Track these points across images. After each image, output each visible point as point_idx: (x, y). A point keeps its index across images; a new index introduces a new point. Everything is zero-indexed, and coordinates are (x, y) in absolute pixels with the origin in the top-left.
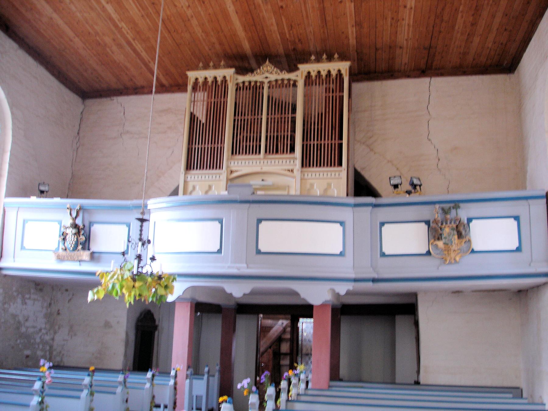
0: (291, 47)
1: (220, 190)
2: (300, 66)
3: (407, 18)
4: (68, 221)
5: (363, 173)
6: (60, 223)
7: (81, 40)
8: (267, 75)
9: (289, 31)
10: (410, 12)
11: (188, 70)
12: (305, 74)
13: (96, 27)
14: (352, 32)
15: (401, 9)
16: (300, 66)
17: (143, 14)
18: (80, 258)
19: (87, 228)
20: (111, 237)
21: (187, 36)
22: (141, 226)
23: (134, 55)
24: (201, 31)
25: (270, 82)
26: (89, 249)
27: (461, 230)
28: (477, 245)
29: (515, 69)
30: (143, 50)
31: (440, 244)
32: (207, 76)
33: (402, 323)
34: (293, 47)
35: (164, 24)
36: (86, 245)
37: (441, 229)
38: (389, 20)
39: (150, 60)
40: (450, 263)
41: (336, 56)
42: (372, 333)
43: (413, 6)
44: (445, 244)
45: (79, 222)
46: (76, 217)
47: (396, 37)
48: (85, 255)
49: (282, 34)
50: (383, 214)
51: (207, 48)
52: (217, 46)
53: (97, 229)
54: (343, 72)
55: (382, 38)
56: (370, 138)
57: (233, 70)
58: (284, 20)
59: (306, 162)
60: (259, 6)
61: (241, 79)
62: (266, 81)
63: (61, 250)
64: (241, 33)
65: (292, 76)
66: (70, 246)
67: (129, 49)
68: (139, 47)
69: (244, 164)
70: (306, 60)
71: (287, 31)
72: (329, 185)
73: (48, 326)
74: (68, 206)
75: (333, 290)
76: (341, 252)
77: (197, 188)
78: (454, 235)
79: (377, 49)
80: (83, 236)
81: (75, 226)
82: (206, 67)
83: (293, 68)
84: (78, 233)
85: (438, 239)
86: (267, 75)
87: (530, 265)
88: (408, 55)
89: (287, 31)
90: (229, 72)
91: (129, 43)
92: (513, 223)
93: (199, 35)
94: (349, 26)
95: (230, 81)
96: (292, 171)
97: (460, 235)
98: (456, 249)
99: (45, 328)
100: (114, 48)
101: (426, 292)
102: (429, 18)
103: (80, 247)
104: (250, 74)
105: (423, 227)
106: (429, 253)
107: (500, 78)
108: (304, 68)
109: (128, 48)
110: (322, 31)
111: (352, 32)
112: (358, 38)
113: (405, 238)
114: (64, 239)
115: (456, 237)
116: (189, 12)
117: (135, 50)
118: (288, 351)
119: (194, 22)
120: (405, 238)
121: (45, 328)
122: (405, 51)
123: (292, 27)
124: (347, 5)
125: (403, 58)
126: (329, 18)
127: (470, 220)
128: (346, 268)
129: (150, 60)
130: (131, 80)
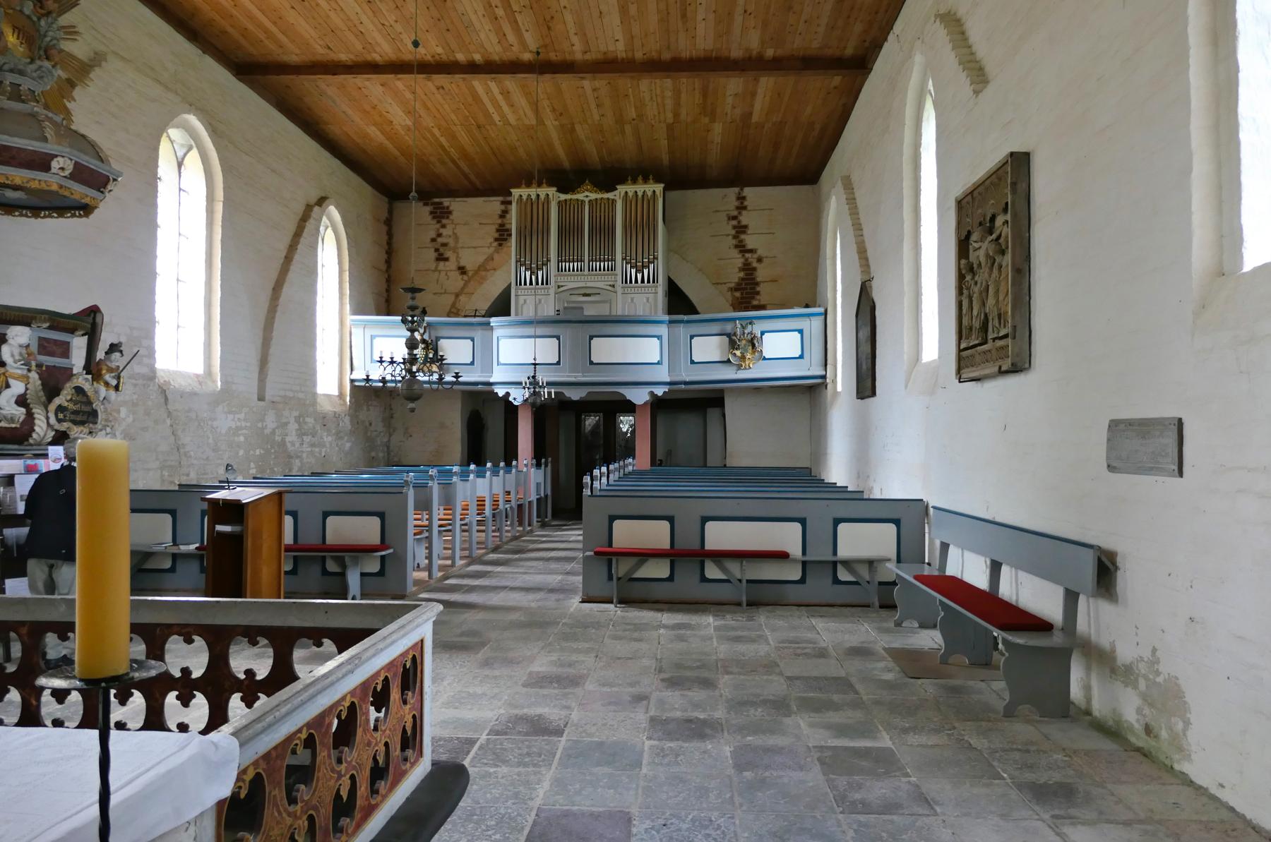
8: (587, 195)
27: (753, 343)
28: (766, 354)
31: (738, 353)
33: (713, 414)
35: (657, 602)
42: (686, 426)
50: (695, 329)
54: (658, 193)
61: (563, 197)
62: (587, 200)
64: (554, 135)
65: (610, 195)
70: (623, 181)
75: (652, 393)
82: (529, 185)
83: (611, 188)
90: (552, 191)
92: (797, 335)
101: (732, 389)
105: (726, 339)
108: (622, 189)
109: (451, 165)
113: (708, 348)
118: (732, 462)
120: (708, 348)
127: (762, 333)
128: (663, 374)
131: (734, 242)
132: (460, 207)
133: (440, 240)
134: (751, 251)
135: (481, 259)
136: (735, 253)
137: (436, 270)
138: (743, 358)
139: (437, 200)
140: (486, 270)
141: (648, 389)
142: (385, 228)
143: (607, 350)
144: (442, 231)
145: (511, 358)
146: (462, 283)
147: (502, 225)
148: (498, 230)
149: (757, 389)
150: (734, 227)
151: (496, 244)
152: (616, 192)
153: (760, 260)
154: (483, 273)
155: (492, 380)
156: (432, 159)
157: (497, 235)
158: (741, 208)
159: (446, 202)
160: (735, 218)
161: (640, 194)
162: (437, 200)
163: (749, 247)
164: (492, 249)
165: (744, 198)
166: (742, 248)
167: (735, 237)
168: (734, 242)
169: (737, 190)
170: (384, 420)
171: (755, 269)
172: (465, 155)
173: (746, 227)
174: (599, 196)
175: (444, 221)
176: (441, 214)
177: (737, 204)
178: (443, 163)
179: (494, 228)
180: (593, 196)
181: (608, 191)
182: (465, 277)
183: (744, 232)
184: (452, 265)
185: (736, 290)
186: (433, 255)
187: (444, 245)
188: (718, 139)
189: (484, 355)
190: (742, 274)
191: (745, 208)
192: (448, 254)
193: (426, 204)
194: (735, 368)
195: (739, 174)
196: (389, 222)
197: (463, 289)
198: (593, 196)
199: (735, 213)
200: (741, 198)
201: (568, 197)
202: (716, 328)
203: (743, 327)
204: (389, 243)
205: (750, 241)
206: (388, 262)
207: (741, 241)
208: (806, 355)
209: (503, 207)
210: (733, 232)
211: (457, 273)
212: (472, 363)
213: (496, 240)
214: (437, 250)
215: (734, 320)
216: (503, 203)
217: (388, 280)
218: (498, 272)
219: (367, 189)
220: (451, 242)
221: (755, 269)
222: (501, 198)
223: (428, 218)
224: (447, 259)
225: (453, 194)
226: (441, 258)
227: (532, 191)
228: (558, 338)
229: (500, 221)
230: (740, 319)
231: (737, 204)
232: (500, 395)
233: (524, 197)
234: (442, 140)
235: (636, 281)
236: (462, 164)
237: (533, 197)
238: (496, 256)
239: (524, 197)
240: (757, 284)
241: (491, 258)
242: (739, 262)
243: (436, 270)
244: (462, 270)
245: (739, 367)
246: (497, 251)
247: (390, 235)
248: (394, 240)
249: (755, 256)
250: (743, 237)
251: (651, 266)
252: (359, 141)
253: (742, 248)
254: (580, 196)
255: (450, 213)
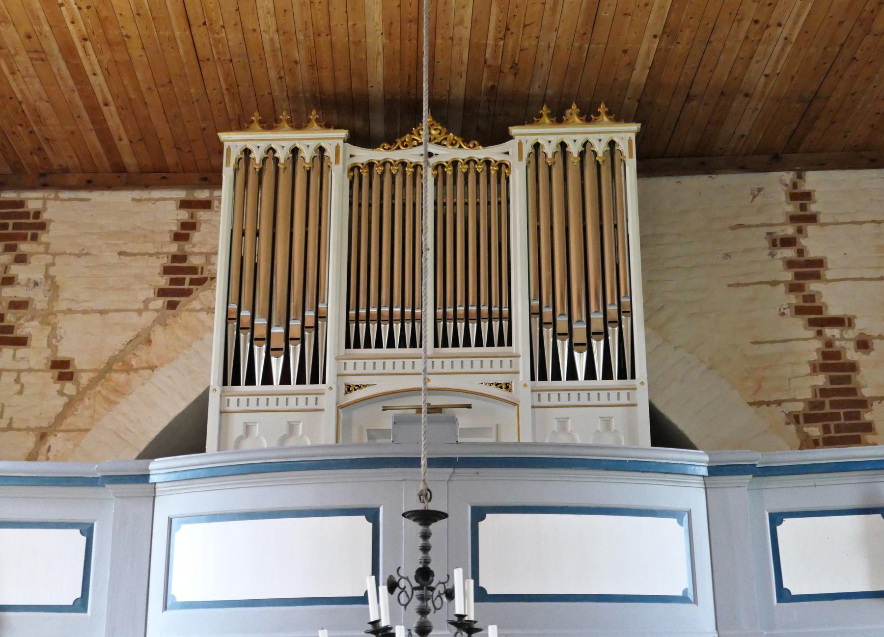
0: (486, 82)
1: (319, 432)
2: (514, 130)
3: (790, 22)
8: (430, 150)
9: (496, 40)
11: (229, 129)
12: (527, 149)
16: (514, 130)
21: (233, 38)
22: (426, 536)
25: (439, 166)
30: (98, 70)
34: (490, 84)
38: (746, 24)
39: (110, 99)
47: (747, 67)
49: (476, 47)
51: (273, 74)
52: (302, 72)
57: (343, 133)
58: (494, 9)
59: (542, 369)
61: (363, 155)
64: (376, 41)
65: (494, 153)
68: (90, 62)
69: (386, 371)
70: (528, 119)
71: (491, 41)
72: (292, 428)
77: (256, 430)
79: (689, 98)
82: (269, 123)
86: (432, 148)
88: (756, 114)
89: (491, 41)
90: (334, 139)
91: (69, 51)
93: (266, 37)
94: (648, 34)
95: (337, 162)
96: (508, 387)
102: (841, 23)
104: (387, 146)
108: (523, 135)
122: (752, 105)
123: (507, 29)
125: (743, 122)
131: (794, 299)
134: (837, 322)
135: (117, 341)
136: (798, 327)
140: (128, 369)
144: (16, 270)
146: (61, 401)
150: (790, 264)
153: (863, 344)
154: (121, 377)
157: (163, 282)
160: (787, 242)
161: (574, 149)
163: (833, 310)
164: (148, 317)
165: (808, 196)
166: (815, 315)
168: (794, 299)
169: (788, 176)
173: (819, 263)
174: (463, 153)
175: (24, 247)
177: (792, 208)
178: (39, 56)
180: (445, 154)
181: (486, 143)
182: (70, 388)
183: (817, 277)
184: (35, 356)
185: (810, 419)
191: (813, 219)
192: (26, 327)
197: (61, 417)
198: (445, 154)
199: (790, 230)
200: (801, 197)
201: (378, 155)
205: (833, 298)
207: (811, 298)
210: (789, 276)
211: (50, 375)
213: (162, 293)
216: (184, 204)
218: (160, 376)
220: (39, 298)
221: (853, 367)
222: (181, 194)
225: (49, 178)
227: (283, 140)
228: (372, 515)
229: (174, 248)
231: (792, 208)
233: (257, 155)
235: (572, 375)
237: (283, 154)
238: (159, 335)
239: (257, 155)
240: (864, 404)
242: (811, 348)
244: (63, 369)
246: (161, 321)
249: (851, 334)
250: (813, 286)
253: (815, 315)
254: (412, 155)
255: (43, 226)
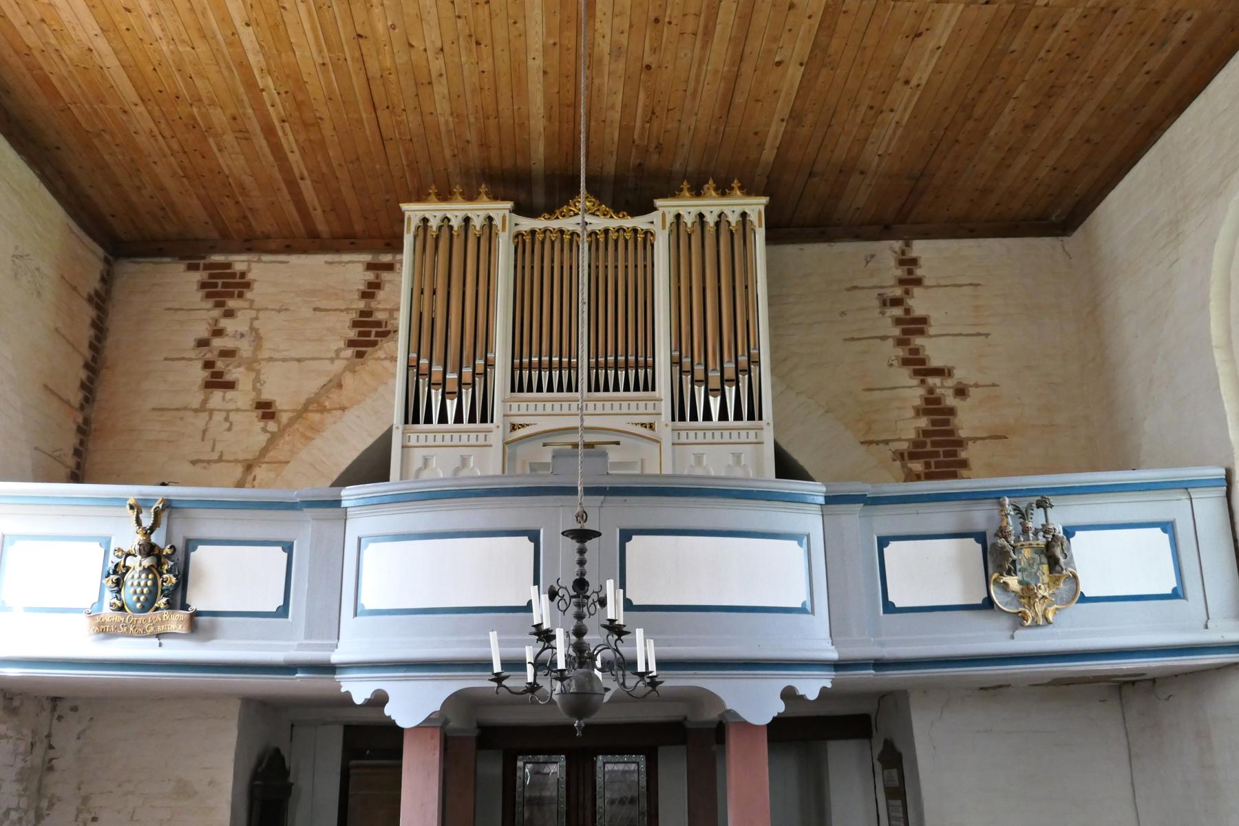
0: (634, 160)
2: (658, 203)
3: (901, 108)
4: (132, 539)
5: (335, 477)
6: (105, 542)
7: (150, 113)
8: (584, 219)
9: (644, 122)
10: (912, 95)
12: (670, 219)
13: (199, 83)
14: (777, 131)
15: (898, 86)
16: (658, 203)
17: (328, 61)
18: (160, 629)
19: (180, 556)
20: (234, 575)
21: (413, 120)
23: (271, 159)
24: (448, 111)
26: (185, 607)
29: (1075, 228)
31: (1013, 582)
32: (427, 215)
34: (638, 161)
36: (177, 597)
37: (1014, 548)
38: (863, 109)
39: (305, 173)
40: (1036, 625)
41: (736, 184)
43: (923, 82)
44: (1020, 582)
45: (158, 538)
46: (152, 529)
48: (176, 621)
49: (626, 129)
51: (448, 153)
52: (474, 150)
53: (202, 556)
55: (832, 151)
56: (785, 360)
58: (642, 96)
60: (600, 61)
61: (527, 224)
63: (107, 609)
64: (538, 124)
65: (640, 222)
66: (135, 598)
67: (264, 143)
69: (547, 412)
71: (638, 124)
73: (24, 803)
74: (131, 501)
75: (789, 695)
76: (1175, 590)
77: (434, 463)
78: (1041, 563)
79: (811, 174)
80: (166, 575)
81: (149, 549)
82: (445, 195)
83: (650, 208)
84: (155, 570)
85: (1009, 573)
87: (1206, 627)
89: (638, 124)
90: (500, 210)
91: (269, 131)
93: (442, 120)
94: (776, 118)
96: (651, 426)
97: (1053, 563)
98: (1046, 594)
99: (17, 809)
100: (229, 138)
101: (927, 688)
102: (946, 109)
103: (162, 602)
105: (974, 547)
106: (989, 604)
107: (1044, 245)
108: (667, 207)
109: (261, 142)
110: (713, 127)
111: (776, 131)
112: (781, 149)
113: (930, 570)
114: (119, 584)
115: (1045, 568)
116: (437, 65)
117: (276, 148)
119: (440, 89)
120: (930, 570)
121: (17, 809)
124: (790, 71)
126: (739, 100)
127: (1069, 532)
129: (305, 173)
130: (245, 217)
131: (901, 352)
132: (268, 273)
133: (217, 343)
134: (939, 372)
135: (311, 386)
136: (904, 376)
137: (202, 408)
138: (1028, 594)
139: (218, 258)
140: (323, 410)
141: (776, 684)
142: (89, 313)
143: (672, 569)
144: (225, 323)
145: (1020, 90)
146: (263, 438)
147: (366, 313)
148: (355, 324)
149: (995, 690)
150: (898, 321)
151: (350, 352)
152: (655, 216)
153: (961, 392)
155: (336, 657)
156: (219, 117)
157: (352, 334)
158: (911, 282)
159: (240, 262)
160: (896, 302)
161: (711, 220)
162: (218, 258)
163: (935, 362)
164: (339, 365)
166: (919, 366)
167: (900, 342)
168: (901, 352)
169: (898, 245)
170: (22, 777)
171: (951, 411)
172: (302, 114)
173: (924, 320)
174: (614, 223)
175: (232, 303)
176: (225, 288)
177: (900, 272)
178: (244, 135)
179: (348, 318)
180: (598, 223)
181: (634, 213)
182: (272, 426)
183: (921, 332)
184: (242, 397)
185: (913, 456)
186: (201, 375)
187: (227, 354)
188: (922, 75)
189: (321, 585)
190: (923, 422)
191: (918, 282)
192: (235, 373)
193: (193, 268)
194: (1005, 622)
195: (911, 208)
196: (100, 301)
197: (265, 451)
198: (598, 223)
199: (898, 292)
200: (909, 263)
201: (539, 224)
202: (944, 516)
203: (1023, 515)
204: (96, 346)
205: (935, 351)
206: (89, 389)
207: (916, 351)
208: (1192, 587)
209: (370, 276)
210: (896, 331)
212: (283, 611)
213: (351, 343)
214: (208, 365)
215: (996, 496)
216: (370, 267)
217: (84, 430)
218: (350, 415)
219: (55, 212)
220: (245, 348)
221: (951, 411)
222: (367, 258)
223: (195, 297)
224: (230, 385)
225: (253, 244)
226: (217, 382)
227: (456, 210)
228: (534, 536)
229: (361, 305)
230: (1011, 493)
231: (900, 272)
232: (358, 699)
233: (434, 224)
234: (248, 37)
235: (708, 416)
236: (288, 140)
237: (456, 223)
238: (348, 380)
239: (434, 224)
240: (960, 443)
241: (337, 384)
242: (915, 394)
243: (202, 408)
244: (266, 410)
245: (1019, 620)
246: (350, 369)
247: (100, 328)
248: (110, 340)
249: (950, 382)
250: (918, 341)
251: (744, 379)
252: (31, 38)
253: (919, 366)
254: (569, 224)
255: (248, 285)
